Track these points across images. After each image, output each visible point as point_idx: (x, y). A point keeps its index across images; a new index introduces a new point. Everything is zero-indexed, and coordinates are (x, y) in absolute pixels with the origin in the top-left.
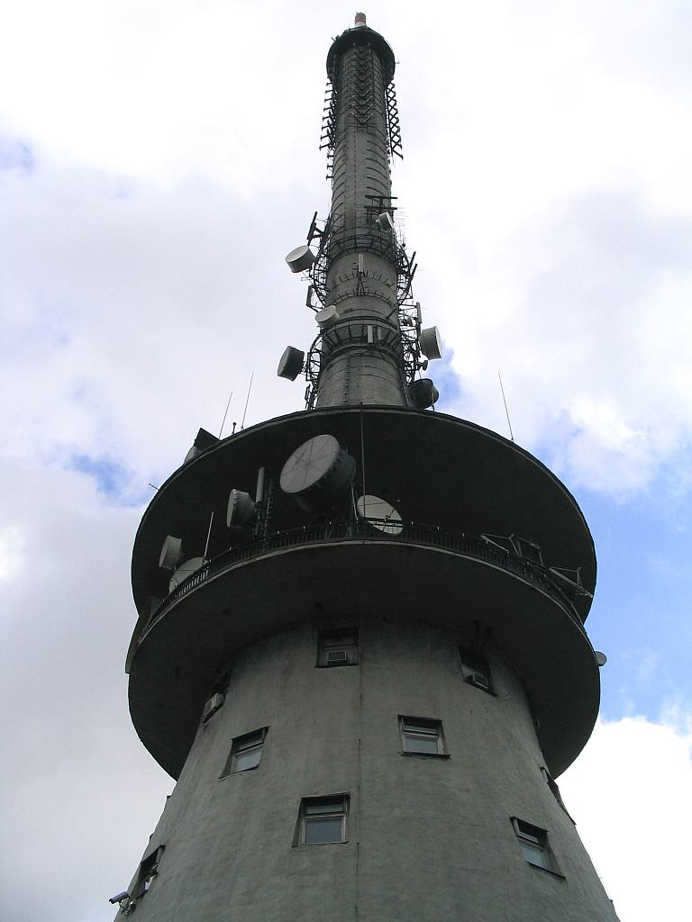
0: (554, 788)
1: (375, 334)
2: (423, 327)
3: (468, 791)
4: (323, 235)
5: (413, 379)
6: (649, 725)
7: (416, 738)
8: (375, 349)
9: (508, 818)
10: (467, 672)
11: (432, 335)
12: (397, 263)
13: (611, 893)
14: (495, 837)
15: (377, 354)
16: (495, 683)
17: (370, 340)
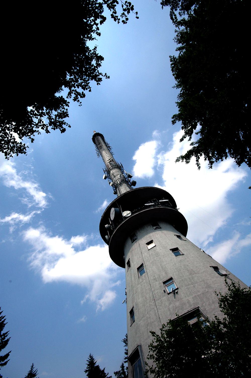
0: (186, 238)
1: (119, 182)
2: (189, 137)
3: (161, 250)
4: (106, 171)
5: (130, 182)
6: (1, 356)
7: (170, 285)
8: (121, 184)
9: (169, 250)
10: (154, 227)
11: (173, 75)
12: (181, 90)
13: (173, 197)
14: (168, 255)
15: (121, 184)
16: (160, 226)
17: (119, 183)
